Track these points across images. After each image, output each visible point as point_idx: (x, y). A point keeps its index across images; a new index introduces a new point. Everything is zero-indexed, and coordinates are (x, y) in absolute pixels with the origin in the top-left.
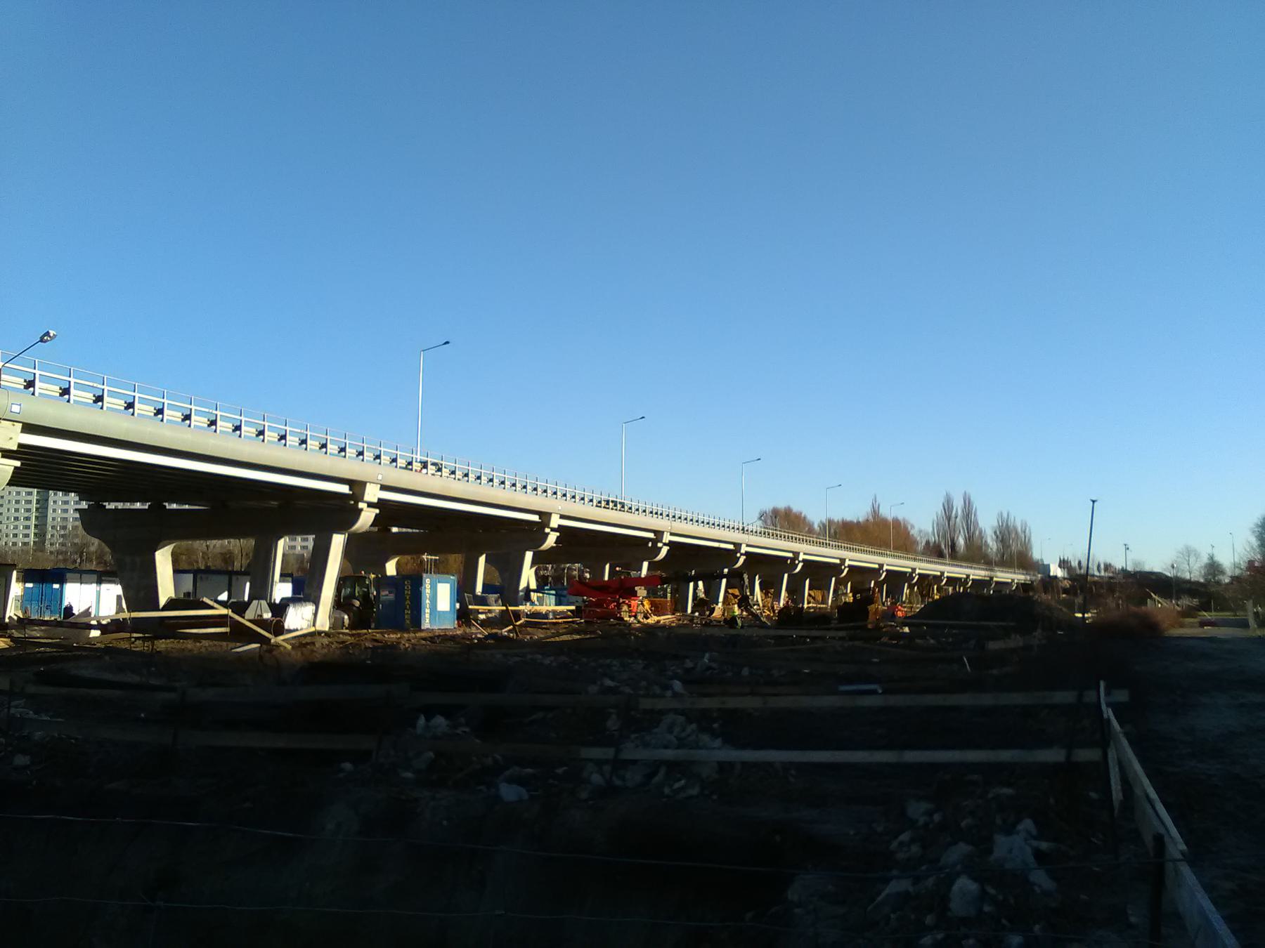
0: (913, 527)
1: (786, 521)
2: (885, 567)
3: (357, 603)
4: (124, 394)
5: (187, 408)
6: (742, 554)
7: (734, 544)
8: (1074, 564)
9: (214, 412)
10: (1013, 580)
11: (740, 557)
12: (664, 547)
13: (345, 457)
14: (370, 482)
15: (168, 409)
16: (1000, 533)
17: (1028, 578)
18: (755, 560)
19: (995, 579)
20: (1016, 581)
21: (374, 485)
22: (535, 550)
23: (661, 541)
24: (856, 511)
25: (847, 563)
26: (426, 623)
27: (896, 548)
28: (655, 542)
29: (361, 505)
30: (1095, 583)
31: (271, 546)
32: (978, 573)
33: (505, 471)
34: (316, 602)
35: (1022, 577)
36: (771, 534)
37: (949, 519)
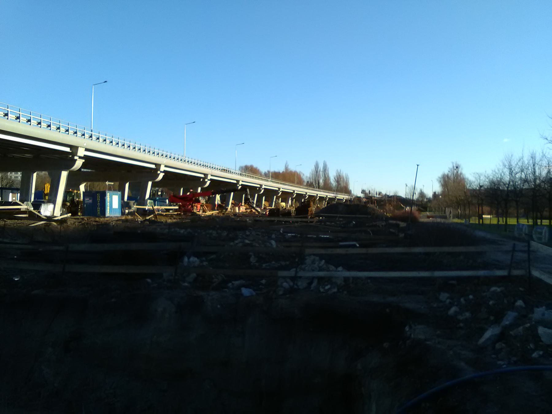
0: (303, 175)
1: (251, 170)
2: (296, 192)
3: (68, 204)
4: (37, 119)
5: (29, 116)
6: (240, 185)
7: (237, 180)
8: (367, 192)
9: (7, 109)
10: (344, 198)
11: (239, 186)
12: (161, 173)
13: (68, 134)
14: (81, 147)
15: (22, 117)
16: (337, 178)
17: (350, 197)
18: (244, 187)
19: (337, 198)
20: (345, 199)
21: (83, 148)
22: (153, 181)
23: (207, 179)
24: (280, 168)
25: (281, 190)
26: (108, 214)
27: (298, 183)
28: (204, 179)
29: (76, 158)
30: (375, 200)
31: (31, 177)
32: (331, 195)
33: (85, 128)
34: (54, 203)
35: (347, 197)
36: (246, 175)
37: (317, 172)
